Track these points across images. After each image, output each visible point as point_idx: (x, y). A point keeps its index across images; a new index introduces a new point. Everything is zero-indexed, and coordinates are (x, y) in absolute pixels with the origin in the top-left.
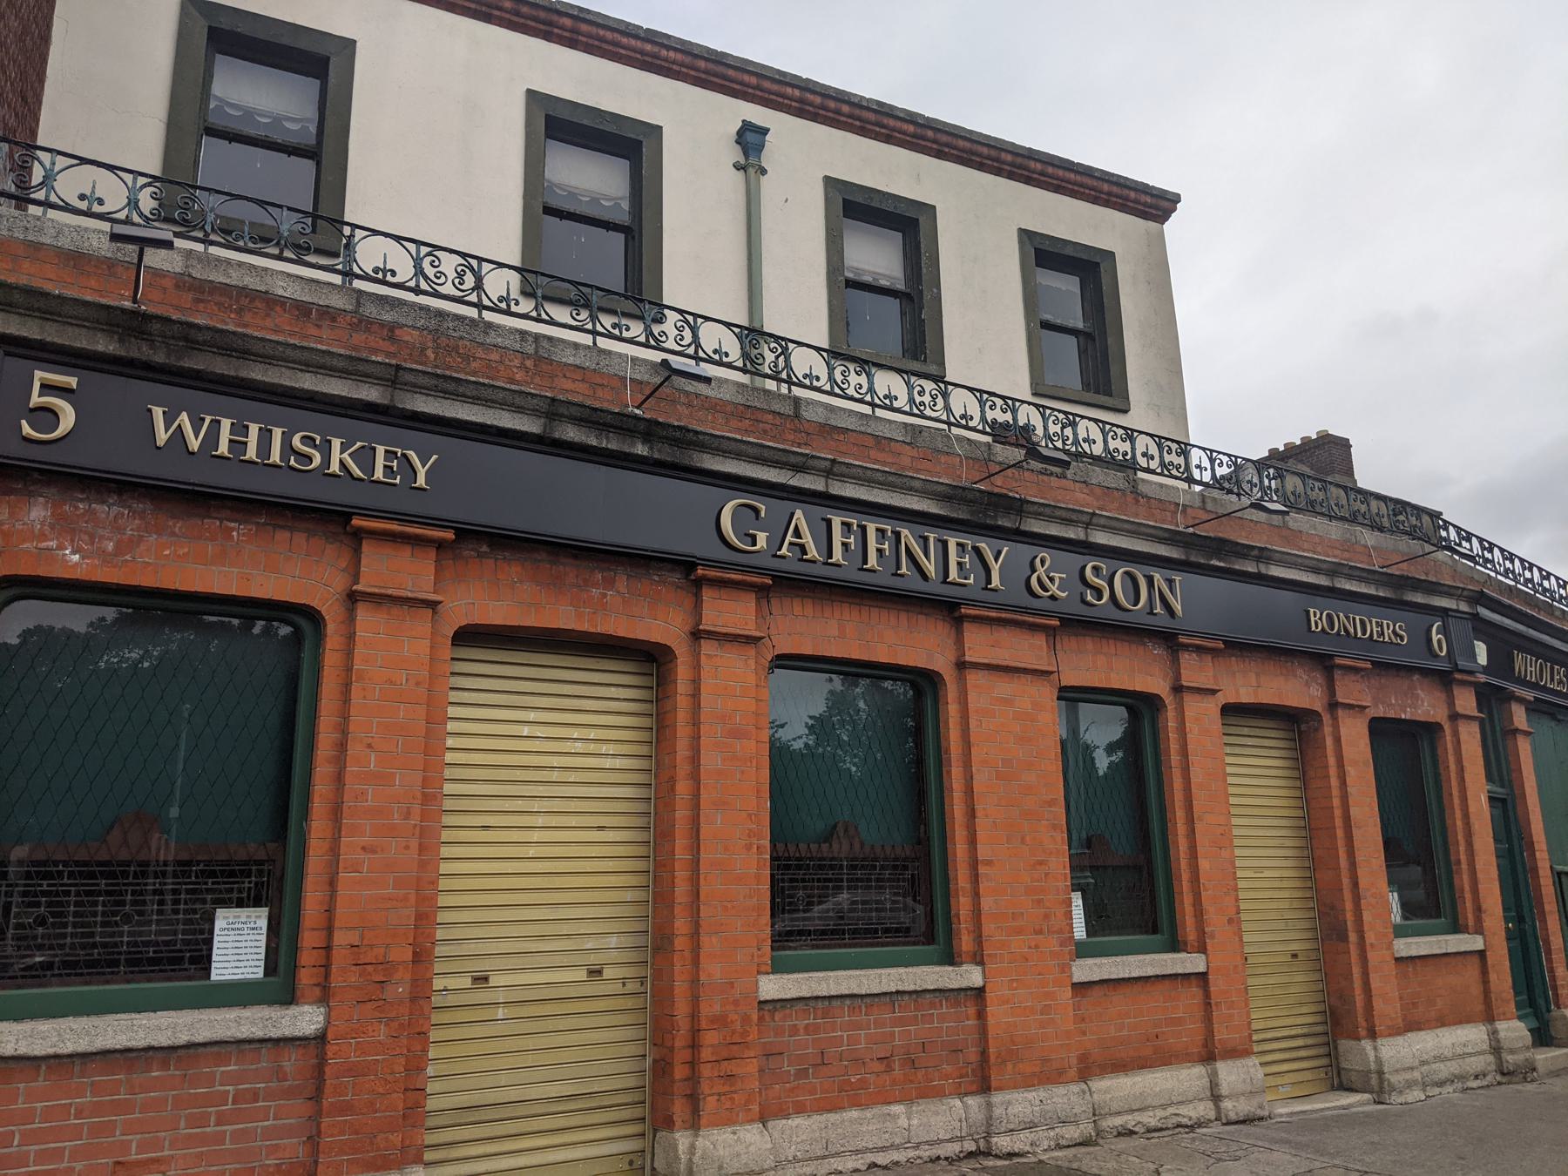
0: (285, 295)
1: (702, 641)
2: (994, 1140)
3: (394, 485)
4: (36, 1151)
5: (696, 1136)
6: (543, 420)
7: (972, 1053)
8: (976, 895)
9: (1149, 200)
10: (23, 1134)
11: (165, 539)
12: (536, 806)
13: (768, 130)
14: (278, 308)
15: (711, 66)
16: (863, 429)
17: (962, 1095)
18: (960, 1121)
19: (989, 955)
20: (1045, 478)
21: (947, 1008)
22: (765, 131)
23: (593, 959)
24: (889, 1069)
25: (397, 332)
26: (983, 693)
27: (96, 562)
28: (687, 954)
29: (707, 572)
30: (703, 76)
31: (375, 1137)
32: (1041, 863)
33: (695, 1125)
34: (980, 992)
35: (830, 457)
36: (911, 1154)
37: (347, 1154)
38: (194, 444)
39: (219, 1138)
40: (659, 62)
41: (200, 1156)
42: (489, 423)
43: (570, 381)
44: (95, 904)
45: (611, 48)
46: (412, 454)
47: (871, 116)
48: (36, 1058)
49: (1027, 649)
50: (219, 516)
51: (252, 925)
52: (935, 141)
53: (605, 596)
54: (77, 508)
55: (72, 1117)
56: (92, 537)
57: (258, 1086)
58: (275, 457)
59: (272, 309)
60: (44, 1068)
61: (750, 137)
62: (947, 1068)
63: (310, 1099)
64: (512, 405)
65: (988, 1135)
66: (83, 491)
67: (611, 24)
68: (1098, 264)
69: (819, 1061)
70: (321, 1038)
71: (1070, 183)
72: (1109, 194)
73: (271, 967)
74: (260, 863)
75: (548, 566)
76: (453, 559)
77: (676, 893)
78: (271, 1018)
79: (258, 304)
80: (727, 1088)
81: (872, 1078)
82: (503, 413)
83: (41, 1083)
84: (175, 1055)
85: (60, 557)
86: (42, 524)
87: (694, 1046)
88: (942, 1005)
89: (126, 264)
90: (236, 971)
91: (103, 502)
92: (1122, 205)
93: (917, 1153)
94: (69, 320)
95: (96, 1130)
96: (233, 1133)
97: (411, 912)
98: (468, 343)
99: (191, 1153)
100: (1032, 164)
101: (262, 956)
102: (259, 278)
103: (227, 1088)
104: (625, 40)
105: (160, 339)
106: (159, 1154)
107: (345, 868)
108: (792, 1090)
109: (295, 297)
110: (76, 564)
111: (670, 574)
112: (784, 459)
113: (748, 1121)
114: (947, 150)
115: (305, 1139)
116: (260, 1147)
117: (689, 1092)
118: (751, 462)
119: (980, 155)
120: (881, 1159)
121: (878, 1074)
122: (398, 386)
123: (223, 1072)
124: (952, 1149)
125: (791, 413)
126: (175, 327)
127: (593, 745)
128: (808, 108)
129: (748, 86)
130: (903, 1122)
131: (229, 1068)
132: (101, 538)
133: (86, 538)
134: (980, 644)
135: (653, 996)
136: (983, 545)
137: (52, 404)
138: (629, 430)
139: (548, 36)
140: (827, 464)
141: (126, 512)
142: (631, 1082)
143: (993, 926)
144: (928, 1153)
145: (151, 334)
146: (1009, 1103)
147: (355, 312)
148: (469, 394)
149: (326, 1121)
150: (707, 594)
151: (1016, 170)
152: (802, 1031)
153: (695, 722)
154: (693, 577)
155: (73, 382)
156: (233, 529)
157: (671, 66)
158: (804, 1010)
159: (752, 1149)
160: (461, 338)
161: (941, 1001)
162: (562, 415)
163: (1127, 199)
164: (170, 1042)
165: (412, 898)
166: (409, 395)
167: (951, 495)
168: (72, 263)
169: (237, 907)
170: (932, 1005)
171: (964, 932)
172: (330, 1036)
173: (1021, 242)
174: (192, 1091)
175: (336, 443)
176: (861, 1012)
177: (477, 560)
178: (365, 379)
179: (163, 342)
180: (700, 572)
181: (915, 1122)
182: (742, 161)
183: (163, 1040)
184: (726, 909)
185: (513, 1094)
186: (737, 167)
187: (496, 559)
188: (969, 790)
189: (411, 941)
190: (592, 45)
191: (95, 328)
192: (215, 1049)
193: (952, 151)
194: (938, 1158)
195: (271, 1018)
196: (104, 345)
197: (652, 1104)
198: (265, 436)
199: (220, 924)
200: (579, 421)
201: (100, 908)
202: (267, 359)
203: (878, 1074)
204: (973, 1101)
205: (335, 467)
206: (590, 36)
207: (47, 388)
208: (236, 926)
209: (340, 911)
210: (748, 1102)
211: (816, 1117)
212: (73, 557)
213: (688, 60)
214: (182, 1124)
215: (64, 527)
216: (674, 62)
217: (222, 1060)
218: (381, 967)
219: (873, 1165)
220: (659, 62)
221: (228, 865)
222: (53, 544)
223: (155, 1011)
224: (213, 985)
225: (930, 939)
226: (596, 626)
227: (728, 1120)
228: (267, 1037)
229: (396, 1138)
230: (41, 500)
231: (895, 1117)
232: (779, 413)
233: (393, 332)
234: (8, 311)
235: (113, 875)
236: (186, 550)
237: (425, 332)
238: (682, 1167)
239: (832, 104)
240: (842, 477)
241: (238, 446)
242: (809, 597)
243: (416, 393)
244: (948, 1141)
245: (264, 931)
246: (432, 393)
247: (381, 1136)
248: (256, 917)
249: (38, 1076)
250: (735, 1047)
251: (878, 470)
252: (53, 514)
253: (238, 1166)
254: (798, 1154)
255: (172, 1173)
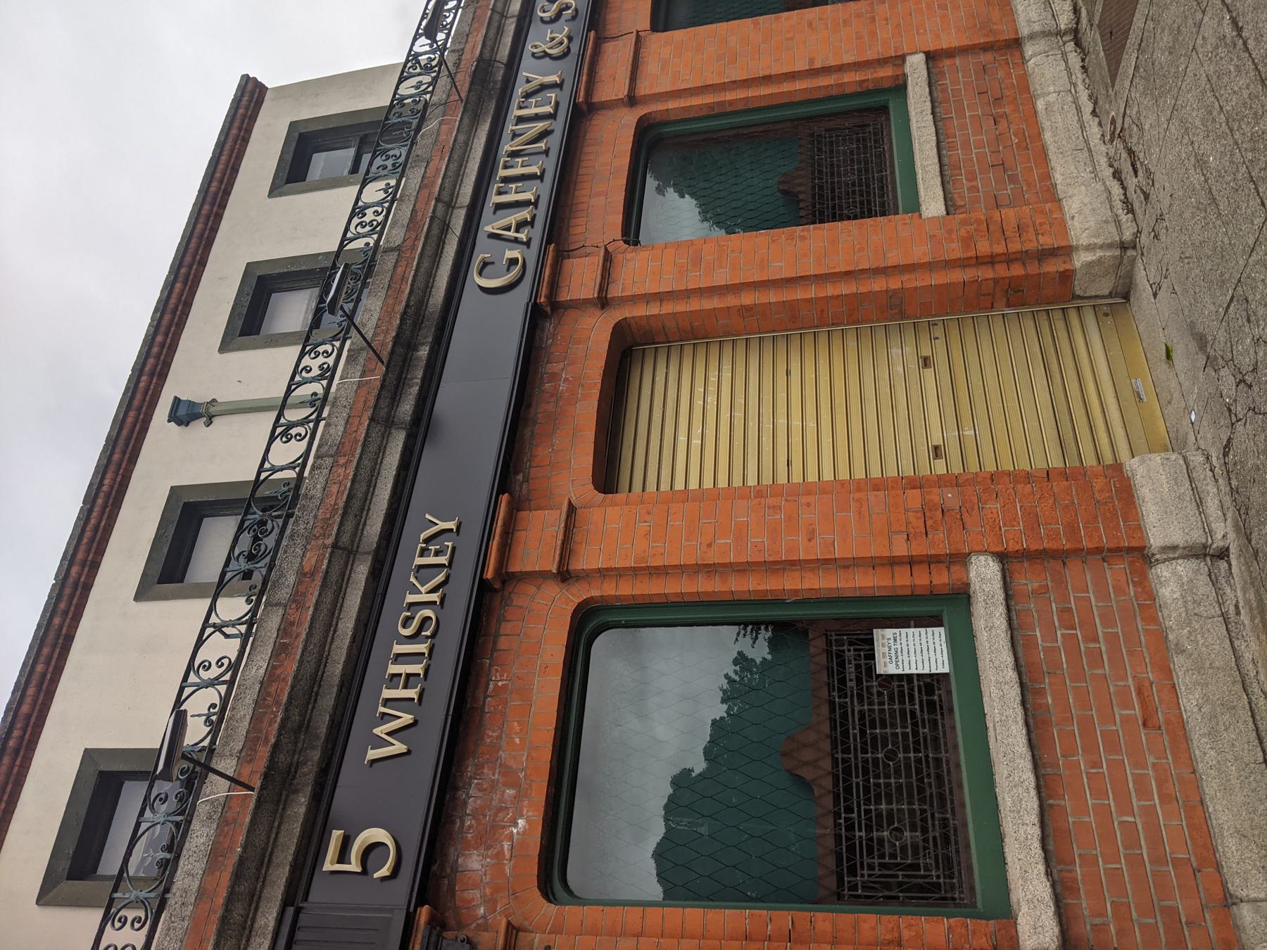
0: (265, 667)
1: (608, 296)
2: (1063, 27)
3: (454, 549)
4: (1139, 800)
5: (1077, 248)
6: (393, 431)
7: (985, 58)
8: (840, 68)
9: (246, 98)
10: (1122, 812)
11: (503, 744)
12: (767, 426)
13: (176, 397)
14: (278, 672)
15: (118, 450)
16: (413, 199)
17: (1024, 61)
18: (1048, 56)
19: (896, 51)
20: (463, 63)
21: (946, 80)
22: (177, 401)
23: (913, 365)
24: (1005, 115)
25: (307, 569)
26: (655, 80)
27: (526, 803)
28: (904, 278)
29: (543, 294)
30: (127, 456)
31: (1098, 502)
32: (810, 24)
33: (1067, 251)
34: (931, 57)
35: (433, 203)
36: (1081, 87)
37: (1118, 524)
38: (407, 718)
39: (1112, 639)
40: (114, 493)
41: (1130, 653)
42: (394, 473)
43: (360, 427)
44: (877, 785)
45: (99, 533)
46: (423, 536)
47: (167, 317)
48: (1041, 806)
49: (616, 57)
50: (482, 699)
51: (892, 641)
52: (190, 267)
53: (566, 380)
54: (470, 827)
55: (1101, 770)
56: (500, 809)
57: (1054, 609)
58: (422, 648)
59: (279, 676)
60: (1051, 802)
61: (182, 412)
62: (1000, 74)
63: (1064, 564)
64: (377, 454)
65: (1059, 33)
66: (453, 823)
67: (77, 533)
68: (300, 135)
69: (1001, 167)
70: (1003, 557)
71: (230, 159)
72: (240, 129)
73: (931, 621)
74: (829, 643)
75: (537, 426)
76: (530, 501)
77: (848, 293)
78: (984, 600)
79: (272, 690)
80: (1031, 230)
81: (1013, 128)
82: (384, 462)
83: (1067, 803)
84: (1029, 684)
85: (520, 837)
86: (485, 857)
87: (991, 260)
88: (943, 84)
89: (225, 810)
90: (938, 651)
91: (465, 803)
92: (250, 118)
93: (1079, 83)
94: (272, 840)
95: (1112, 746)
96: (1104, 625)
97: (872, 496)
98: (321, 511)
99: (1129, 661)
100: (212, 189)
101: (923, 630)
102: (247, 691)
103: (1059, 635)
104: (93, 521)
105: (296, 756)
106: (1132, 689)
107: (830, 552)
108: (1028, 185)
109: (267, 658)
110: (528, 821)
111: (546, 330)
112: (435, 239)
113: (1061, 210)
114: (198, 257)
115: (1105, 564)
116: (1117, 602)
117: (1036, 262)
118: (438, 267)
119: (204, 230)
120: (1087, 107)
121: (1009, 123)
122: (355, 549)
123: (1042, 641)
124: (1074, 59)
125: (396, 254)
126: (284, 741)
127: (710, 388)
128: (158, 369)
129: (137, 419)
130: (1052, 98)
131: (1038, 634)
132: (501, 801)
133: (501, 815)
134: (612, 86)
135: (947, 314)
136: (520, 90)
137: (360, 847)
138: (404, 361)
139: (88, 587)
140: (440, 205)
141: (476, 781)
142: (1029, 324)
143: (869, 52)
144: (1079, 75)
145: (291, 764)
146: (1028, 21)
147: (286, 606)
148: (365, 488)
149: (1086, 543)
150: (564, 296)
151: (218, 202)
152: (973, 183)
153: (687, 294)
154: (548, 309)
155: (337, 834)
156: (496, 686)
157: (117, 483)
158: (953, 184)
159: (1086, 200)
160: (315, 517)
161: (940, 85)
162: (389, 414)
163: (244, 116)
164: (1016, 686)
165: (857, 495)
166: (364, 540)
167: (473, 114)
168: (221, 859)
169: (874, 659)
170: (945, 90)
171: (875, 75)
172: (999, 549)
173: (281, 195)
174: (1065, 666)
175: (411, 598)
176: (953, 142)
177: (531, 482)
178: (347, 577)
179: (300, 754)
180: (542, 300)
181: (1051, 89)
182: (205, 419)
183: (1014, 693)
184: (861, 249)
185: (1047, 414)
186: (209, 424)
187: (530, 466)
188: (745, 83)
189: (900, 492)
190: (97, 549)
191: (282, 816)
192: (1020, 650)
193: (200, 253)
194: (1083, 67)
195: (984, 600)
196: (300, 807)
197: (1049, 303)
198: (399, 658)
199: (892, 670)
200: (395, 399)
201: (882, 781)
202: (322, 660)
203: (1009, 123)
204: (1029, 50)
205: (435, 597)
206: (88, 552)
207: (343, 857)
208: (893, 655)
209: (873, 552)
210: (1043, 212)
211: (1053, 164)
212: (520, 825)
213: (112, 468)
214: (1100, 671)
215: (488, 838)
216: (114, 480)
217: (1031, 643)
218: (928, 514)
219: (1094, 113)
220: (114, 493)
221: (839, 795)
222: (506, 845)
223: (985, 715)
224: (955, 669)
225: (883, 110)
226: (595, 383)
227: (1062, 225)
228: (1004, 602)
229: (1098, 484)
230: (460, 861)
231: (1048, 105)
232: (396, 263)
233: (306, 573)
234: (260, 897)
235: (847, 771)
236: (516, 724)
237: (308, 547)
238: (1108, 254)
239: (155, 350)
240: (454, 195)
241: (409, 679)
242: (569, 221)
243: (362, 534)
244: (1066, 62)
245: (897, 631)
246: (363, 520)
247: (1096, 495)
248: (883, 638)
249: (1059, 805)
250: (992, 228)
251: (447, 166)
252: (476, 848)
253: (1138, 618)
254: (1088, 170)
255: (1150, 675)
